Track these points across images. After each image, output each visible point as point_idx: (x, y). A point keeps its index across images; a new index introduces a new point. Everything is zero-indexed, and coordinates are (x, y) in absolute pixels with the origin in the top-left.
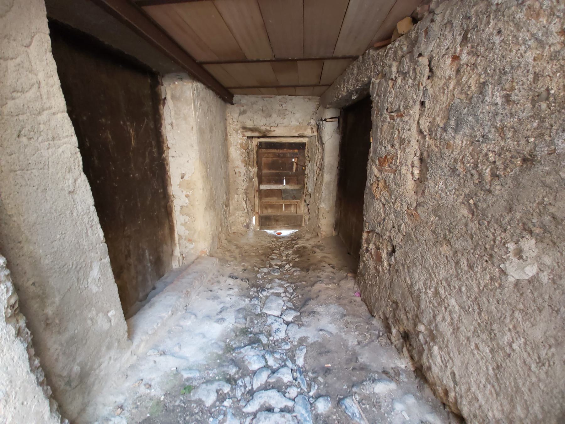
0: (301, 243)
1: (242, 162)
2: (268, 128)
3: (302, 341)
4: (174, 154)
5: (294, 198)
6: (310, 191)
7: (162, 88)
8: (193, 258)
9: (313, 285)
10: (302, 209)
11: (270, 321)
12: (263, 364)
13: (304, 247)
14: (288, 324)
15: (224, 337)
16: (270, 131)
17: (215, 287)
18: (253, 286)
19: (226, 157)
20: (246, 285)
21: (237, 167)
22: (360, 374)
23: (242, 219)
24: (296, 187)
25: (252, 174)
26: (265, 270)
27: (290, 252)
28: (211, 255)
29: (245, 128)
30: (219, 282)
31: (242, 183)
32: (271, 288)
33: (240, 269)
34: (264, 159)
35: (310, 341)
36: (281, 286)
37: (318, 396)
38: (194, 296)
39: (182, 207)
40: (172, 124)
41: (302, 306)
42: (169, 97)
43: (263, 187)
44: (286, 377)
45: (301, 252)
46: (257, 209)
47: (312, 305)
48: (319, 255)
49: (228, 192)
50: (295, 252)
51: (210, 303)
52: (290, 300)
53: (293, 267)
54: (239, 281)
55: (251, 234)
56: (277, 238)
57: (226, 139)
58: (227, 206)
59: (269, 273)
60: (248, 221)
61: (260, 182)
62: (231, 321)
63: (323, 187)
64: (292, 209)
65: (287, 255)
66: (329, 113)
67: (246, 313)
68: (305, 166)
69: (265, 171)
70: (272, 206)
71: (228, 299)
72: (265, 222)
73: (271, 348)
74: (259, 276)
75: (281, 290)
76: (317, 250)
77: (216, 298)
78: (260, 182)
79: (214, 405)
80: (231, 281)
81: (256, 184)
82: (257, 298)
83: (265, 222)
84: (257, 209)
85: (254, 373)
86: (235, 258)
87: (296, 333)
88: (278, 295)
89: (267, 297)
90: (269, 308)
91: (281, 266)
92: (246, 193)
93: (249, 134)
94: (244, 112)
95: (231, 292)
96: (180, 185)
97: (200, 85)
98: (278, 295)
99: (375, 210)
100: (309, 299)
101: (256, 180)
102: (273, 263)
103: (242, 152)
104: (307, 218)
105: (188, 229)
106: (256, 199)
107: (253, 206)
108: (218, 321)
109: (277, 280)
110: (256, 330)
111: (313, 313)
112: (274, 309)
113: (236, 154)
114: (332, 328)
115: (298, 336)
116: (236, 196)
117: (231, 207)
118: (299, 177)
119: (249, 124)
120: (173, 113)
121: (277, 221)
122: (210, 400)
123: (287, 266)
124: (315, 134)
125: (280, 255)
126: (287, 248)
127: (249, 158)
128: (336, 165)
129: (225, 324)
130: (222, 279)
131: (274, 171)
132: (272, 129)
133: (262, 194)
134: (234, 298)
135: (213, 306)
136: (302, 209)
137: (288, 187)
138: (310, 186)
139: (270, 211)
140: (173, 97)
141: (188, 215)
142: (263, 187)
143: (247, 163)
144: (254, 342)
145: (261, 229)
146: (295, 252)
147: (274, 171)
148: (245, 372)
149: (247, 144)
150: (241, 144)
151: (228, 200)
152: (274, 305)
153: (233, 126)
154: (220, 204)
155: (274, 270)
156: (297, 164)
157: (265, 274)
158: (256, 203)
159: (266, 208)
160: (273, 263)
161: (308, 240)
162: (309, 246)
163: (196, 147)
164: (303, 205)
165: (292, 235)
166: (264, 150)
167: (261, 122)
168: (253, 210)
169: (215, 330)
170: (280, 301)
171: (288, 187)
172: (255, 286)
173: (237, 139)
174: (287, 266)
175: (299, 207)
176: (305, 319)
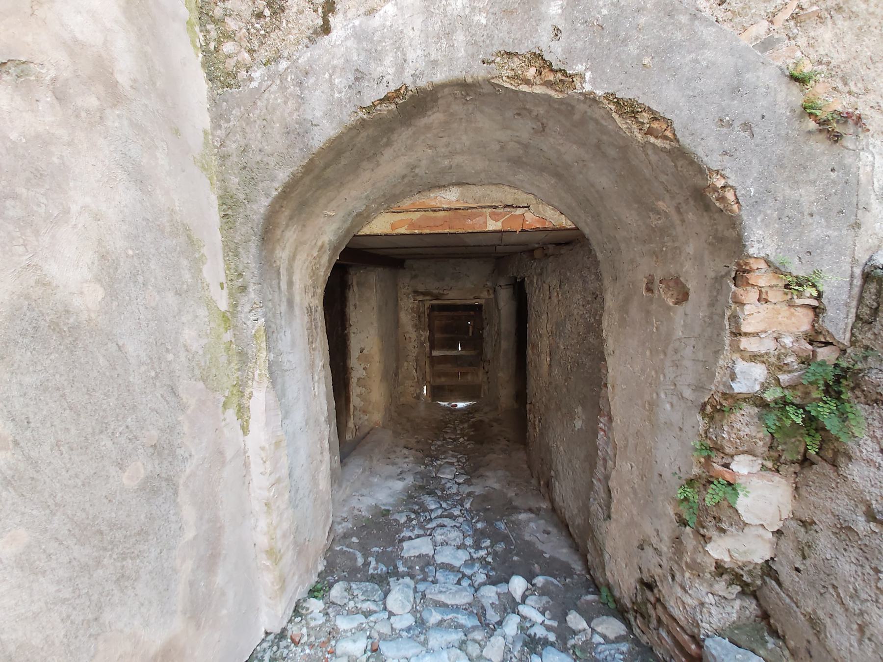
0: (478, 416)
1: (413, 326)
2: (441, 292)
3: (469, 494)
4: (355, 331)
5: (471, 364)
6: (488, 356)
7: (350, 276)
8: (367, 430)
9: (484, 456)
10: (481, 377)
11: (443, 482)
12: (438, 506)
13: (481, 421)
14: (459, 484)
15: (406, 489)
16: (443, 294)
17: (392, 456)
18: (427, 456)
19: (397, 322)
20: (420, 455)
21: (408, 332)
22: (511, 509)
23: (412, 389)
24: (473, 353)
25: (422, 338)
26: (439, 443)
27: (466, 426)
28: (384, 427)
29: (416, 292)
30: (395, 452)
31: (412, 350)
32: (445, 458)
33: (413, 441)
34: (437, 323)
35: (477, 494)
36: (453, 456)
37: (477, 522)
38: (375, 462)
39: (359, 379)
40: (355, 305)
41: (472, 472)
42: (354, 283)
43: (435, 353)
44: (456, 512)
45: (477, 426)
46: (428, 378)
47: (481, 471)
48: (496, 428)
49: (398, 360)
50: (470, 427)
51: (390, 467)
52: (463, 468)
53: (468, 440)
54: (413, 451)
55: (422, 407)
56: (453, 410)
57: (396, 305)
58: (396, 375)
59: (442, 445)
60: (418, 391)
61: (432, 348)
62: (410, 480)
63: (501, 355)
64: (469, 378)
65: (461, 430)
66: (502, 282)
67: (422, 475)
68: (483, 329)
69: (438, 336)
70: (446, 374)
71: (405, 465)
72: (437, 392)
73: (445, 498)
74: (433, 448)
75: (454, 460)
76: (495, 424)
77: (394, 464)
78: (432, 348)
79: (406, 522)
80: (406, 451)
81: (428, 349)
82: (432, 465)
83: (437, 392)
84: (428, 378)
85: (432, 510)
86: (408, 431)
87: (466, 489)
88: (452, 464)
89: (441, 465)
90: (443, 473)
91: (454, 440)
92: (417, 360)
93: (421, 298)
94: (415, 276)
95: (407, 460)
96: (358, 358)
97: (380, 269)
98: (452, 464)
99: (532, 383)
100: (480, 467)
101: (427, 345)
102: (447, 436)
103: (413, 317)
104: (486, 387)
105: (364, 400)
106: (427, 366)
107: (424, 375)
108: (399, 480)
109: (451, 452)
110: (432, 487)
111: (481, 476)
112: (447, 475)
113: (406, 319)
114: (497, 486)
115: (466, 492)
116: (405, 364)
117: (400, 376)
118: (476, 342)
119: (421, 288)
120: (357, 296)
121: (451, 391)
122: (403, 520)
123: (461, 440)
124: (492, 296)
125: (455, 428)
126: (462, 422)
127: (420, 321)
128: (513, 331)
129: (406, 482)
130: (398, 450)
131: (448, 336)
132: (445, 292)
133: (433, 361)
134: (410, 465)
135: (395, 470)
136: (481, 377)
137: (464, 353)
138: (489, 353)
139: (443, 379)
140: (358, 284)
141: (364, 386)
142: (435, 353)
143: (417, 327)
144: (431, 493)
145: (433, 401)
146: (470, 427)
147: (448, 336)
148: (425, 510)
149: (418, 307)
150: (412, 309)
151: (397, 368)
152: (447, 471)
153: (404, 291)
154: (392, 375)
155: (448, 443)
156: (473, 327)
157: (439, 446)
158: (428, 370)
159: (439, 376)
160: (447, 436)
161: (486, 413)
162: (487, 420)
163: (375, 325)
164: (481, 373)
165: (468, 407)
166: (436, 313)
167: (433, 286)
168: (424, 378)
169: (399, 485)
170: (453, 468)
171: (464, 353)
172: (428, 455)
173: (408, 303)
174: (461, 440)
175: (477, 375)
176: (474, 481)
